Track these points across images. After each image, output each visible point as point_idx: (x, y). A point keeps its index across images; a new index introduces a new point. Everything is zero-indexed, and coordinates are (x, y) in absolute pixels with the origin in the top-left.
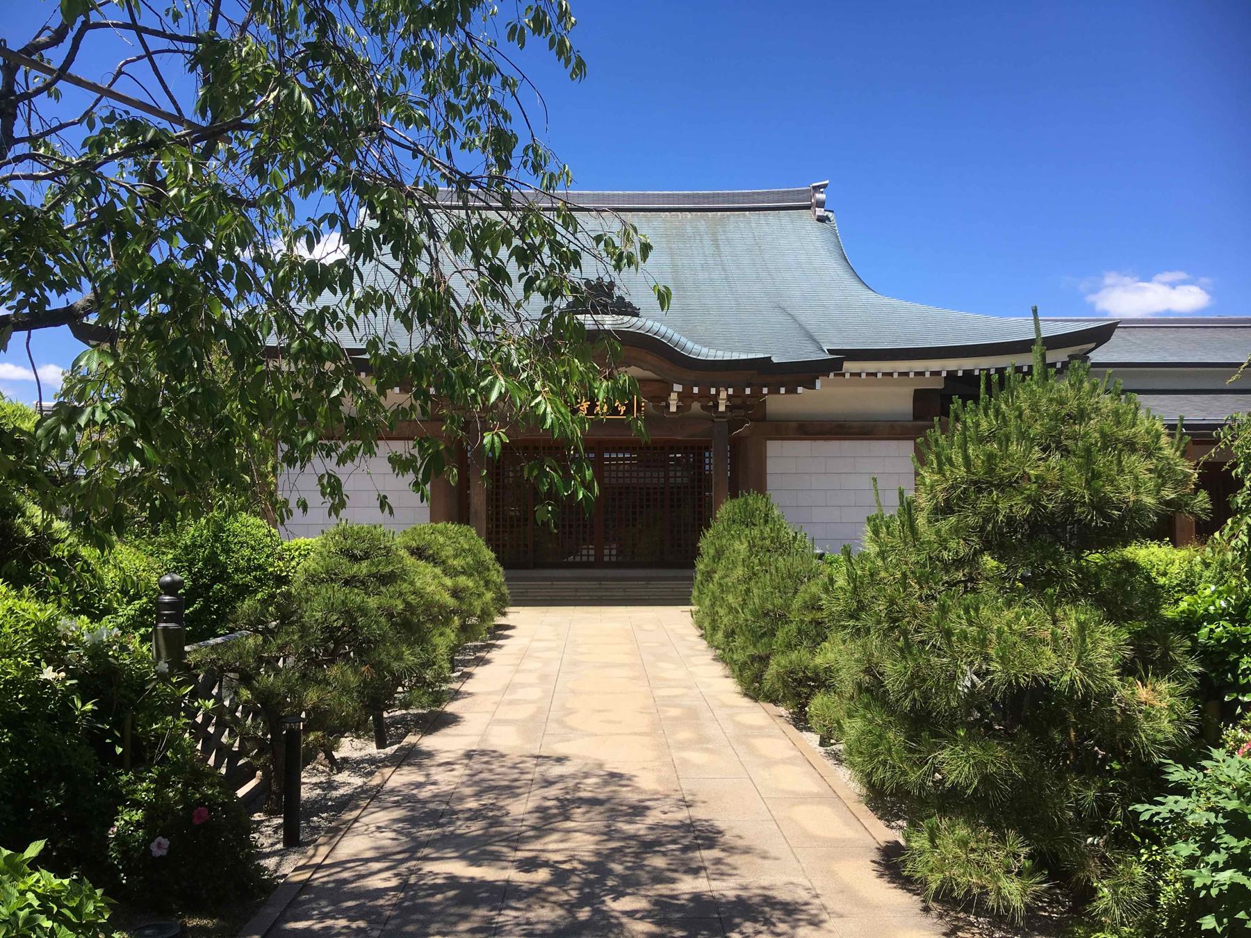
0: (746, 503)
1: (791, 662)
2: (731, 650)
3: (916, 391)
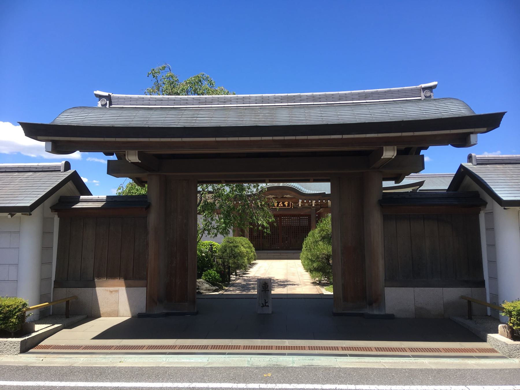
3: (108, 173)
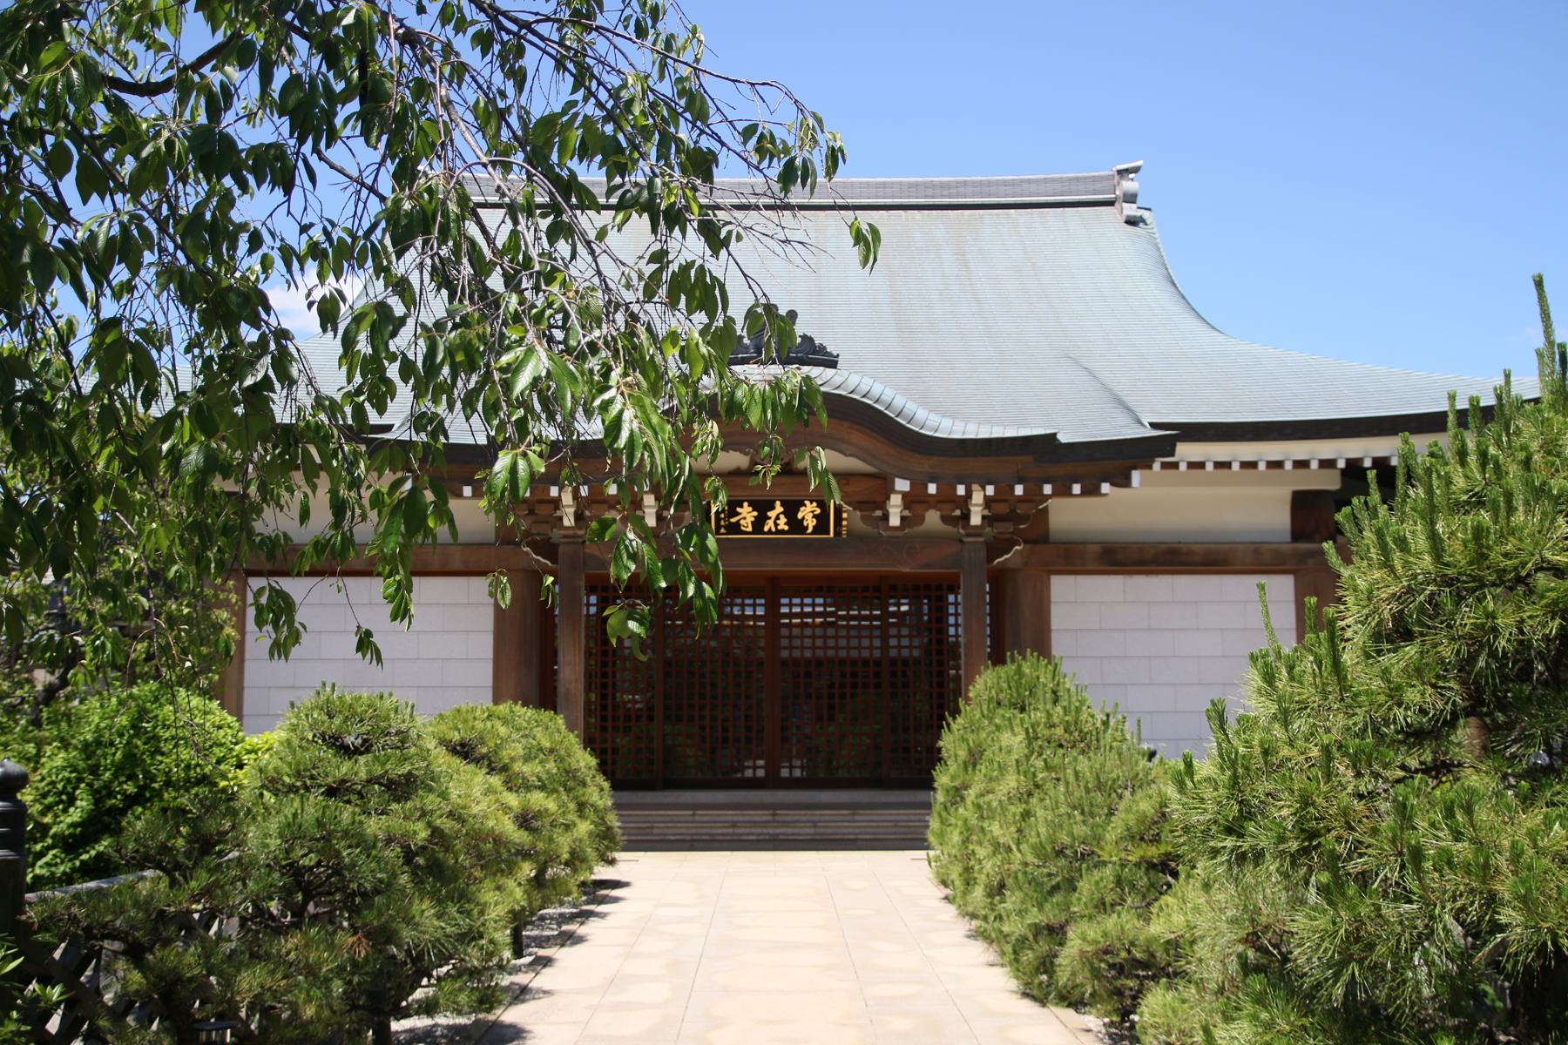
0: (1019, 672)
1: (1105, 934)
2: (999, 918)
